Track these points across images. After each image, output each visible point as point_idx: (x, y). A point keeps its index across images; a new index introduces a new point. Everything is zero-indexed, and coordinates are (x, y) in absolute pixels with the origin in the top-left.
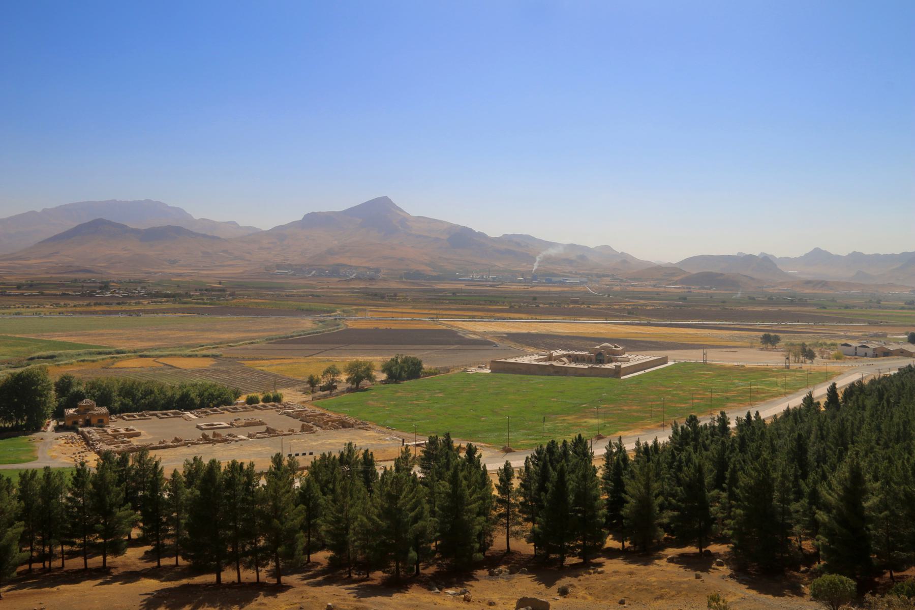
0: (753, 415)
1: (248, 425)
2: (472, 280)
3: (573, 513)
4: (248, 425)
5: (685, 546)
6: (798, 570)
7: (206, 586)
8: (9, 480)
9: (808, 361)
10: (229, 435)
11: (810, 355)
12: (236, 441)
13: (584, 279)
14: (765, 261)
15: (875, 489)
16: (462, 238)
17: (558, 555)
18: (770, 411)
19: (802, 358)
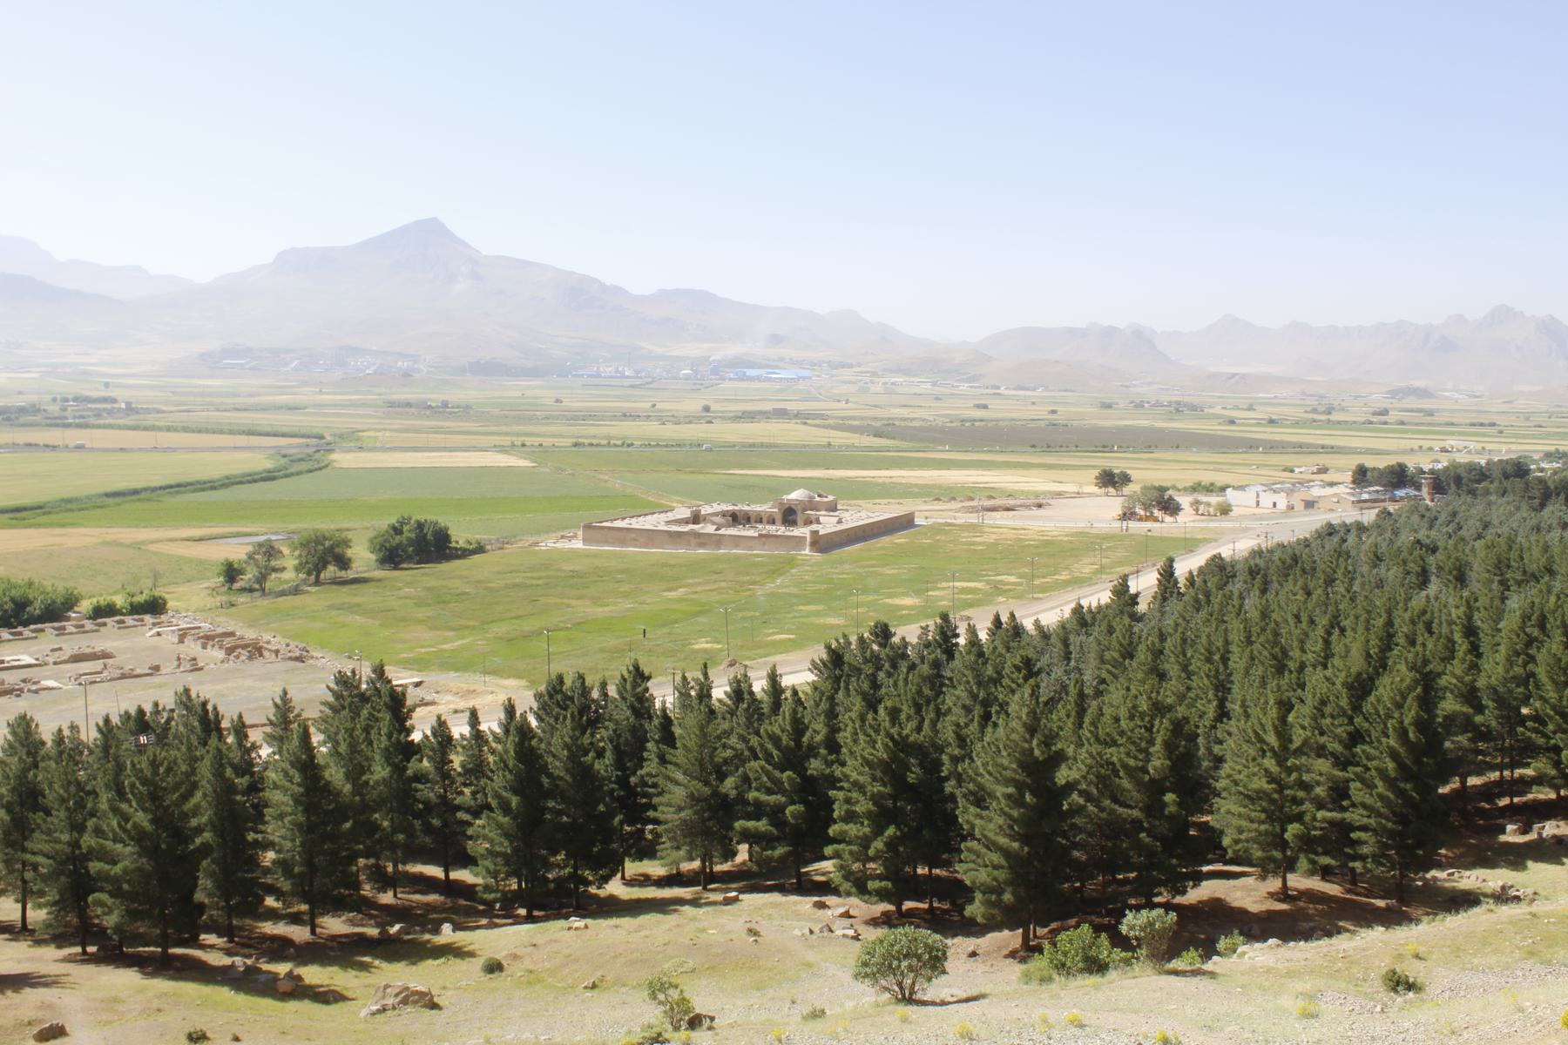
0: (1004, 619)
1: (77, 658)
2: (598, 376)
3: (579, 814)
4: (77, 658)
5: (1484, 785)
6: (1504, 832)
7: (151, 956)
8: (240, 729)
9: (1168, 519)
10: (24, 681)
11: (1171, 507)
12: (36, 692)
13: (806, 373)
14: (1141, 339)
15: (757, 789)
16: (582, 295)
17: (1444, 790)
18: (1049, 613)
19: (1157, 513)
